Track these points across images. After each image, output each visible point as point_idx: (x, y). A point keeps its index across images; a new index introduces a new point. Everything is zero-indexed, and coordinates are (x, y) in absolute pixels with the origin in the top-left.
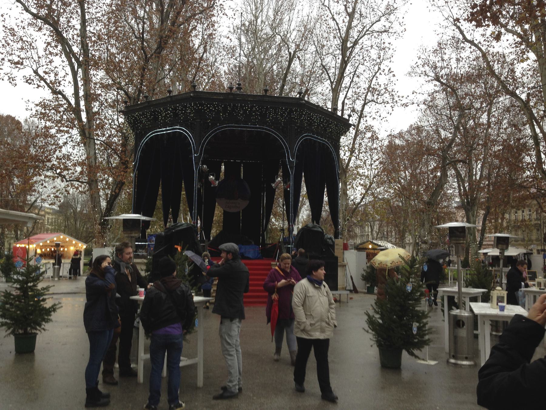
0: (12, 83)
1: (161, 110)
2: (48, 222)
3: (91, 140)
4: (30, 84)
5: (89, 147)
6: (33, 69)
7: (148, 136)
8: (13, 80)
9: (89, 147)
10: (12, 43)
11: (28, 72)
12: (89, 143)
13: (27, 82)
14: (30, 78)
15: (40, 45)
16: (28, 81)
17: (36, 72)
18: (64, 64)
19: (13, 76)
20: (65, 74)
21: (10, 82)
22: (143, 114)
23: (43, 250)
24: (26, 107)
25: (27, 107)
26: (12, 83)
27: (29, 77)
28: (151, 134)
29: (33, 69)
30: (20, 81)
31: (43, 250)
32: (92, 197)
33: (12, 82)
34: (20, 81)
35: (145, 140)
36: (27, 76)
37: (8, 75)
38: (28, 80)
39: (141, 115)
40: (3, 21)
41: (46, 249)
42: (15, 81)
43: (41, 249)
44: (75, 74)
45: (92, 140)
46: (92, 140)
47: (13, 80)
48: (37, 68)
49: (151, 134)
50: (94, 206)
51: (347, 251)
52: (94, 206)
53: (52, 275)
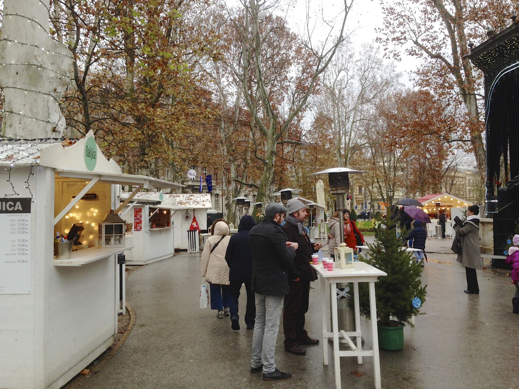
0: (397, 59)
1: (505, 43)
2: (469, 183)
3: (471, 96)
4: (413, 55)
5: (470, 103)
6: (413, 40)
7: (498, 78)
8: (397, 56)
9: (470, 103)
10: (392, 22)
11: (410, 45)
12: (470, 99)
13: (410, 54)
14: (412, 50)
15: (418, 16)
16: (412, 53)
17: (416, 43)
18: (442, 27)
19: (397, 52)
20: (444, 36)
21: (395, 59)
22: (488, 53)
23: (430, 210)
24: (409, 78)
25: (411, 78)
26: (397, 59)
27: (411, 49)
28: (500, 74)
29: (413, 40)
30: (404, 55)
31: (430, 210)
32: (477, 155)
33: (397, 58)
34: (404, 55)
35: (495, 82)
36: (409, 48)
37: (393, 52)
38: (411, 52)
39: (485, 55)
40: (381, 4)
41: (433, 209)
42: (399, 57)
43: (428, 209)
44: (451, 32)
45: (472, 97)
46: (472, 97)
47: (397, 56)
48: (417, 39)
49: (500, 74)
50: (480, 163)
51: (126, 257)
52: (480, 163)
53: (435, 234)
